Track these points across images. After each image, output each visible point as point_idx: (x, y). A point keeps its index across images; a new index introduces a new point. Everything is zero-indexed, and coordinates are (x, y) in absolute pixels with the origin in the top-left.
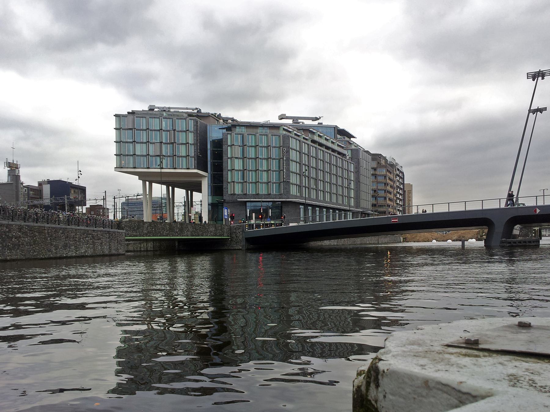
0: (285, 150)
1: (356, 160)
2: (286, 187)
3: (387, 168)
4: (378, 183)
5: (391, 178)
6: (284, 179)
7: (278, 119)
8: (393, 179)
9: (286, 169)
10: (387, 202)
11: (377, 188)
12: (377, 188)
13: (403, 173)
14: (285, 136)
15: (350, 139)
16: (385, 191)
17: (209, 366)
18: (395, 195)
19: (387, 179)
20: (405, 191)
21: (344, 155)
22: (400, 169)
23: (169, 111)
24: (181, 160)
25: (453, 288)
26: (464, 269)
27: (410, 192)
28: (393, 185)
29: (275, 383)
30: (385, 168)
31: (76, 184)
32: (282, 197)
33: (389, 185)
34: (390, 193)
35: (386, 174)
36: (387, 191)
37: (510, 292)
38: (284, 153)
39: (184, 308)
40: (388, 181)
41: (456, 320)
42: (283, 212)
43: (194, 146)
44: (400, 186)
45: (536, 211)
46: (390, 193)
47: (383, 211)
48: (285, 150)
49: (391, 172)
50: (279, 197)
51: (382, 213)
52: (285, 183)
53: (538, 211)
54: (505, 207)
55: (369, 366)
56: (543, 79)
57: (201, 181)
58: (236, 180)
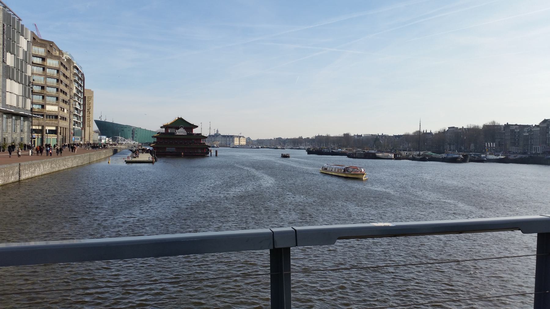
3: (61, 61)
4: (46, 76)
5: (65, 100)
8: (70, 78)
10: (59, 103)
13: (83, 75)
18: (70, 112)
19: (60, 74)
20: (85, 97)
22: (79, 69)
25: (227, 303)
26: (495, 261)
27: (91, 98)
28: (70, 84)
30: (58, 59)
31: (54, 170)
35: (60, 68)
36: (59, 90)
37: (220, 202)
41: (88, 261)
43: (538, 130)
44: (78, 94)
47: (54, 114)
51: (50, 117)
55: (8, 243)
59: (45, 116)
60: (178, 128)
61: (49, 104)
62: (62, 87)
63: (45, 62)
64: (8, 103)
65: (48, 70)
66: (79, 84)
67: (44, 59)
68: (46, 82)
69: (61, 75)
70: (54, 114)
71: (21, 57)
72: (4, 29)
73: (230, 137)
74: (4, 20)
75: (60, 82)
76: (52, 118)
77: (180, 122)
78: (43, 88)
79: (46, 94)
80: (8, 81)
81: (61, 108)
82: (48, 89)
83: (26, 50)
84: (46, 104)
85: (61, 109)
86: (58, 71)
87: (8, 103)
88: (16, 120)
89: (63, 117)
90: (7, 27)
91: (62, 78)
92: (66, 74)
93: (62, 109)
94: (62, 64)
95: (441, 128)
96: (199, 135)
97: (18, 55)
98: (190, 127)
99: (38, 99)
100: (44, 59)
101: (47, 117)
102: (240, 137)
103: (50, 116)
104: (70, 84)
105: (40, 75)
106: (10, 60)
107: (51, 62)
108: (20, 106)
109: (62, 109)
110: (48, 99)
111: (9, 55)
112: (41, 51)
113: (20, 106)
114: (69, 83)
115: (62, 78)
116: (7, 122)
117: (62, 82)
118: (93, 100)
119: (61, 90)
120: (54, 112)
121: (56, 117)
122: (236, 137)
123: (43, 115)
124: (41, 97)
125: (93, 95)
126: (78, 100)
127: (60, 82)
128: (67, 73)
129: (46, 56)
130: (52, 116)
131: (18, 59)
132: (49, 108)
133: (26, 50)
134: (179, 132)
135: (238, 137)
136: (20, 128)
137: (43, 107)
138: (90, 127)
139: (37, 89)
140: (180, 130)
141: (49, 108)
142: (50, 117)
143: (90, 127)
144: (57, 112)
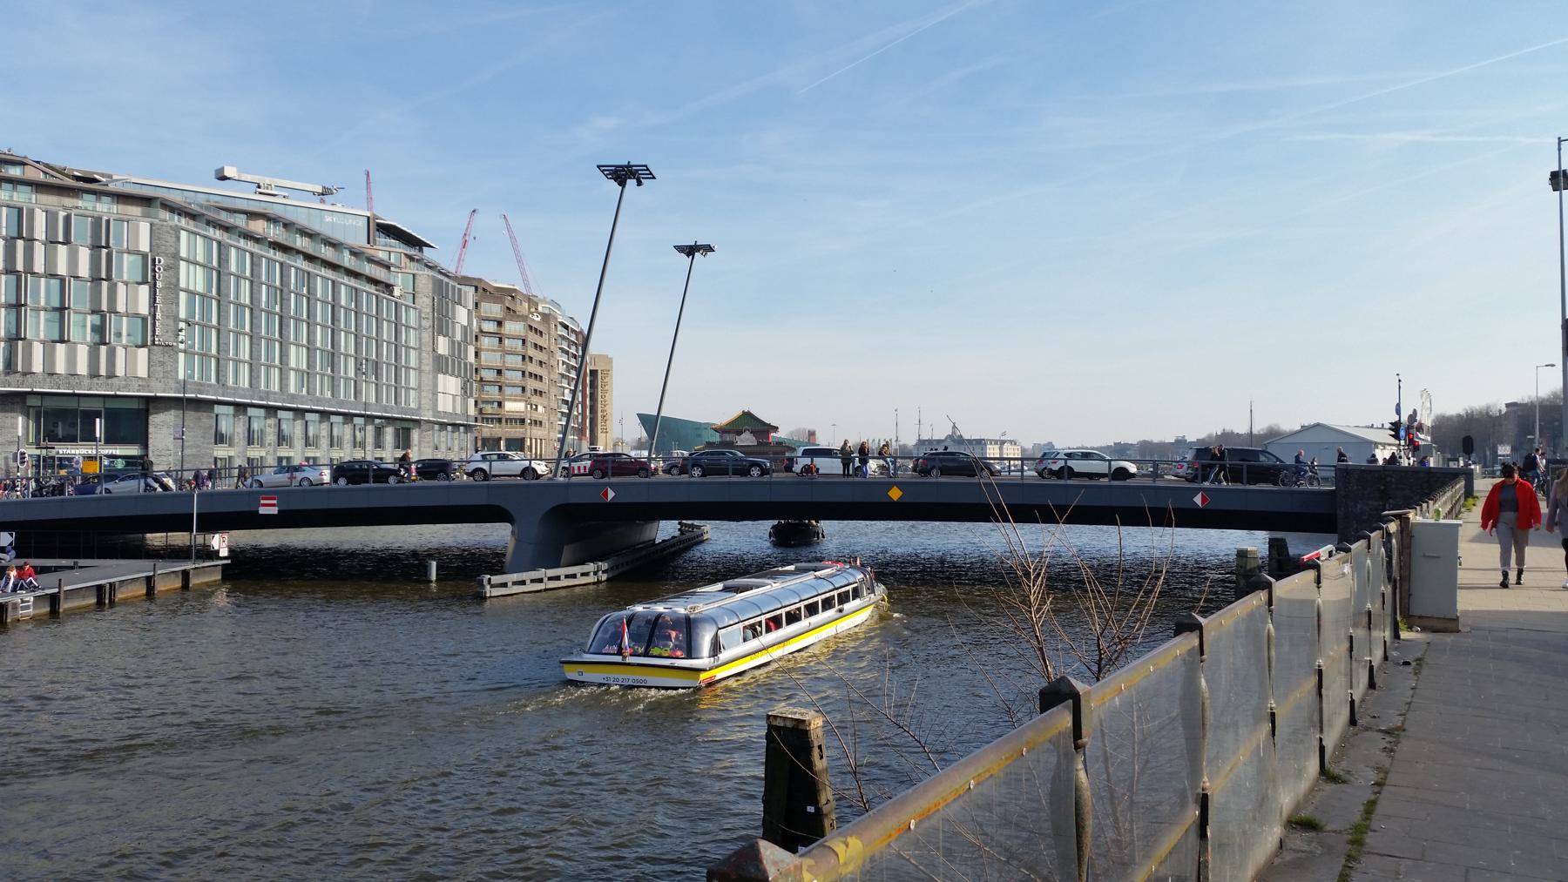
0: (160, 262)
2: (161, 359)
4: (506, 353)
6: (157, 339)
7: (214, 176)
8: (549, 347)
9: (162, 312)
11: (504, 365)
12: (504, 365)
16: (523, 373)
17: (620, 632)
21: (389, 288)
22: (570, 326)
24: (39, 294)
29: (1240, 604)
32: (148, 386)
34: (539, 378)
36: (527, 374)
38: (159, 269)
39: (767, 525)
42: (150, 426)
45: (606, 494)
46: (539, 378)
48: (160, 262)
49: (541, 332)
50: (139, 386)
51: (511, 422)
52: (162, 348)
53: (611, 494)
54: (146, 494)
56: (639, 183)
58: (74, 336)
59: (504, 421)
60: (739, 433)
61: (509, 400)
62: (532, 368)
63: (503, 329)
64: (440, 409)
65: (507, 342)
66: (570, 355)
67: (500, 324)
68: (504, 362)
69: (529, 348)
70: (518, 416)
71: (458, 337)
72: (434, 305)
73: (974, 442)
74: (434, 292)
75: (527, 359)
76: (516, 422)
77: (748, 421)
78: (499, 372)
79: (504, 383)
80: (441, 376)
81: (531, 405)
82: (508, 374)
83: (466, 324)
84: (505, 400)
85: (531, 407)
86: (524, 342)
87: (440, 409)
88: (453, 432)
89: (536, 421)
90: (438, 299)
91: (531, 352)
92: (539, 343)
93: (534, 407)
94: (531, 327)
95: (1468, 408)
96: (779, 443)
97: (454, 336)
98: (762, 429)
99: (493, 392)
100: (500, 324)
101: (506, 422)
102: (1003, 442)
103: (511, 420)
104: (549, 359)
105: (494, 351)
106: (443, 346)
107: (512, 327)
108: (458, 411)
109: (534, 407)
110: (508, 391)
111: (441, 338)
112: (495, 310)
113: (458, 411)
114: (546, 358)
115: (531, 352)
116: (439, 436)
117: (531, 358)
118: (612, 376)
119: (531, 374)
120: (517, 412)
121: (522, 421)
122: (991, 443)
123: (500, 421)
124: (497, 388)
125: (612, 367)
126: (569, 384)
127: (527, 359)
128: (542, 342)
129: (505, 318)
130: (516, 420)
131: (453, 342)
132: (510, 406)
133: (466, 324)
134: (742, 441)
135: (996, 442)
136: (459, 444)
137: (500, 404)
138: (607, 432)
139: (489, 375)
140: (743, 436)
141: (510, 406)
142: (511, 422)
143: (607, 432)
144: (523, 412)
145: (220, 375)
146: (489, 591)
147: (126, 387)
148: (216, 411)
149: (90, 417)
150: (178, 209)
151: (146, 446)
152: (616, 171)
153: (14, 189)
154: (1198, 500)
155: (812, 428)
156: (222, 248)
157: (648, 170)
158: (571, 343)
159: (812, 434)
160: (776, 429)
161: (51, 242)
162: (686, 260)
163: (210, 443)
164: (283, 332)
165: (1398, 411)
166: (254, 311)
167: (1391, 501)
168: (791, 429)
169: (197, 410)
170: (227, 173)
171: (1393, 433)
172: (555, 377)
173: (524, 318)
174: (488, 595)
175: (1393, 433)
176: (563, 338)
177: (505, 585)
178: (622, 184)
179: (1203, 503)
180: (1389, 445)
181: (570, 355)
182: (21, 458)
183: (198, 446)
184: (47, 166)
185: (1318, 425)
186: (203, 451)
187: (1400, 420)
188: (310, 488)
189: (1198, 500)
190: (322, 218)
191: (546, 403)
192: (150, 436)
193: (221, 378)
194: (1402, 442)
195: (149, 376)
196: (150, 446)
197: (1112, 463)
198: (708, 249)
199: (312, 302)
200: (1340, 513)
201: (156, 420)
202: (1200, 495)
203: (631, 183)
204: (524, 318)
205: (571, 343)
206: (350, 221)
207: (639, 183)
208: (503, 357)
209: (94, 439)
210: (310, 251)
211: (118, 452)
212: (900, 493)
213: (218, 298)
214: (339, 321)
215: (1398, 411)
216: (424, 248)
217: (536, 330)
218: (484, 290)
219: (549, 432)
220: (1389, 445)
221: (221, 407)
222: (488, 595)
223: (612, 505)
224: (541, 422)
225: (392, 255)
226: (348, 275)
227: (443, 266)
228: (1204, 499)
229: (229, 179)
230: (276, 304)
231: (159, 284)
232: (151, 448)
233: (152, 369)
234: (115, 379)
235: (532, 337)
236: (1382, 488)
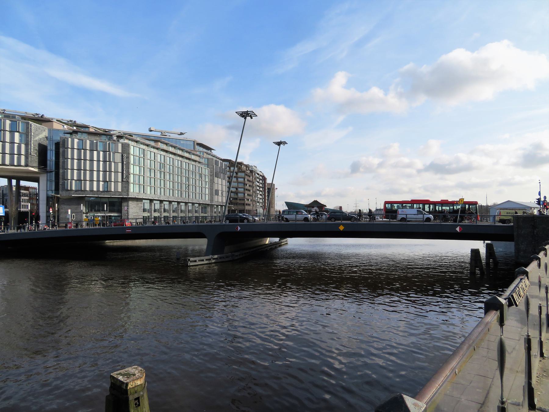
1: (212, 166)
14: (125, 144)
15: (211, 151)
23: (3, 113)
33: (248, 185)
38: (125, 158)
40: (246, 182)
45: (237, 228)
51: (240, 204)
53: (239, 228)
56: (252, 118)
57: (39, 177)
59: (238, 204)
60: (313, 207)
66: (260, 183)
78: (237, 189)
82: (239, 189)
94: (246, 174)
104: (253, 184)
142: (240, 204)
145: (145, 190)
146: (190, 264)
147: (115, 195)
148: (143, 202)
149: (103, 204)
150: (143, 143)
151: (121, 213)
152: (242, 114)
153: (82, 134)
154: (458, 229)
155: (341, 206)
156: (145, 151)
157: (253, 113)
158: (260, 179)
159: (341, 208)
160: (325, 206)
161: (92, 151)
162: (277, 147)
163: (141, 212)
164: (165, 177)
165: (540, 194)
166: (165, 173)
167: (537, 229)
168: (334, 206)
169: (137, 201)
170: (152, 129)
171: (538, 200)
172: (254, 190)
173: (244, 172)
174: (189, 265)
175: (538, 200)
176: (258, 178)
177: (195, 261)
178: (245, 118)
179: (460, 230)
180: (536, 208)
181: (260, 183)
182: (73, 217)
183: (138, 213)
184: (95, 128)
185: (509, 201)
186: (139, 214)
187: (540, 198)
188: (248, 223)
189: (458, 229)
190: (180, 142)
191: (252, 198)
192: (122, 210)
193: (145, 191)
194: (541, 206)
195: (122, 191)
196: (122, 212)
197: (407, 215)
198: (285, 143)
199: (182, 169)
200: (515, 234)
201: (124, 205)
202: (458, 227)
203: (248, 118)
204: (244, 172)
205: (260, 179)
206: (188, 143)
207: (252, 118)
208: (238, 184)
209: (104, 211)
210: (174, 152)
211: (112, 215)
212: (343, 228)
213: (139, 165)
214: (183, 173)
215: (540, 194)
216: (212, 150)
217: (248, 175)
218: (232, 163)
219: (253, 208)
220: (536, 208)
221: (165, 202)
222: (189, 265)
223: (239, 232)
224: (250, 205)
225: (201, 153)
226: (193, 161)
227: (217, 156)
228: (460, 229)
229: (152, 131)
230: (163, 168)
231: (125, 163)
232: (122, 214)
233: (123, 189)
234: (111, 192)
235: (247, 178)
236: (533, 224)
